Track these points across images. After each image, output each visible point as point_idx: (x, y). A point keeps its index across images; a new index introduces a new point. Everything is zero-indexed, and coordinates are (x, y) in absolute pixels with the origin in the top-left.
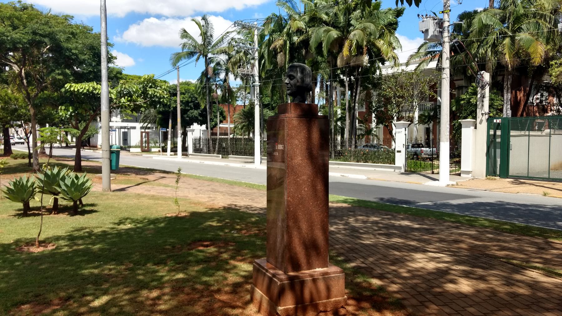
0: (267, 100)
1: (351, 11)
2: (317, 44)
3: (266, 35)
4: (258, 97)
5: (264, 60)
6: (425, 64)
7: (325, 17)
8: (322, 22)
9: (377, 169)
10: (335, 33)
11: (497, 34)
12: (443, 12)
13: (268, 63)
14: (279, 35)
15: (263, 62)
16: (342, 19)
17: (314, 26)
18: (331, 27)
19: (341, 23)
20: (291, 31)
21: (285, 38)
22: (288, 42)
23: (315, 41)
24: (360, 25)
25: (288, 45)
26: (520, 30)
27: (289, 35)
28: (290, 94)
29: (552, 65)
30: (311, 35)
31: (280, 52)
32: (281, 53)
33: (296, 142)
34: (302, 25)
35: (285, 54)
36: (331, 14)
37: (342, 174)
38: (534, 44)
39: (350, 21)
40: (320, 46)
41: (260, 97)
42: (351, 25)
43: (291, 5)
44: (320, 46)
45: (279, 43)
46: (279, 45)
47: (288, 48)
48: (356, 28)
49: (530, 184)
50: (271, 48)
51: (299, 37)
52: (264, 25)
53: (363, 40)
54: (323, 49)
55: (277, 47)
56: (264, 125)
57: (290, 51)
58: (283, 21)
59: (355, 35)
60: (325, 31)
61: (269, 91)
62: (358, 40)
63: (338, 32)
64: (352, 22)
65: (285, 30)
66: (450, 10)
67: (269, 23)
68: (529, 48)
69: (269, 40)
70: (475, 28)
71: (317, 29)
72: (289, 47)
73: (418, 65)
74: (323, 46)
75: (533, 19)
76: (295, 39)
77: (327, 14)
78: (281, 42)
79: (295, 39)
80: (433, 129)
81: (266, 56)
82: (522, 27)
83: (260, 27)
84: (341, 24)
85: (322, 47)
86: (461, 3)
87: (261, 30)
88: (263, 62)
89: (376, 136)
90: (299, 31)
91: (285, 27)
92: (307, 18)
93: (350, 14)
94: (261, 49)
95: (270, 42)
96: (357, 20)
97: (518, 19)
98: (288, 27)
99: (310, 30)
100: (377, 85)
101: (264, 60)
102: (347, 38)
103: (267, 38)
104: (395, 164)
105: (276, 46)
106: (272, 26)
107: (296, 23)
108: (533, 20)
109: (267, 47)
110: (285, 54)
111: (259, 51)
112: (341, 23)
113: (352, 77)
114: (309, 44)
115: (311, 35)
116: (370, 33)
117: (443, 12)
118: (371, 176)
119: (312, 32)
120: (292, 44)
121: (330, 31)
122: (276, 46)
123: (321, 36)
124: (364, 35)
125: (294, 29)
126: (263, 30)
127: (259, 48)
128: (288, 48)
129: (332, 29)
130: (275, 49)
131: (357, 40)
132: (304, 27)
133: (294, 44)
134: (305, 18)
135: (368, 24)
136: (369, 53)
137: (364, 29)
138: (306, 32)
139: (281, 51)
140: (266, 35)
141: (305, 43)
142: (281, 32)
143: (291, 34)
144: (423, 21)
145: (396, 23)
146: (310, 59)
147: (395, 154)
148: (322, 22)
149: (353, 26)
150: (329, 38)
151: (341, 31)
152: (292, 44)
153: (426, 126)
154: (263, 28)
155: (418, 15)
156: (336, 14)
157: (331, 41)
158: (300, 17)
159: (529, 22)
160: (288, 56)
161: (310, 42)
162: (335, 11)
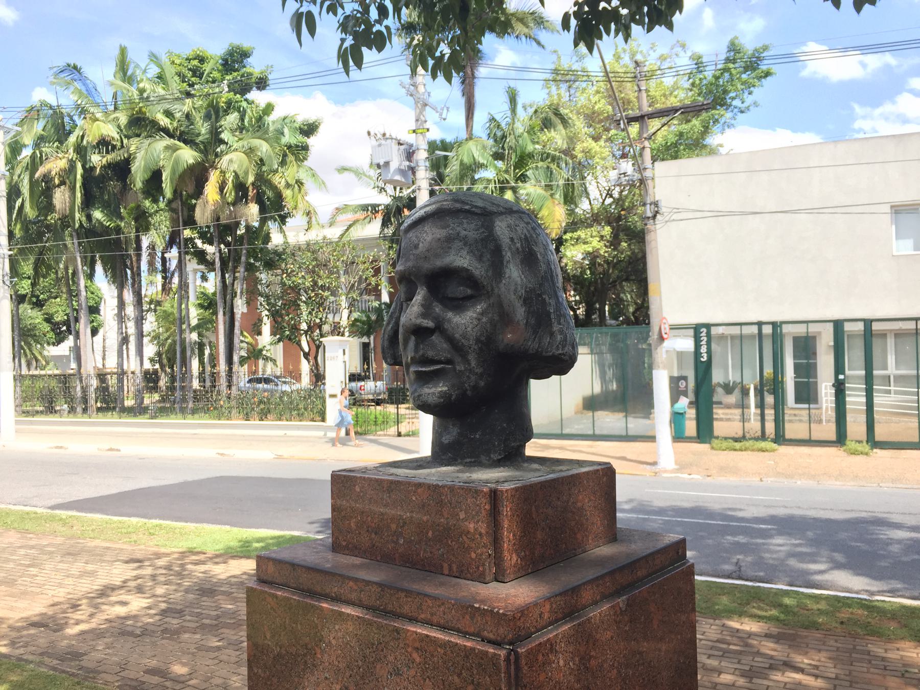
0: (25, 286)
1: (221, 114)
2: (149, 174)
3: (25, 146)
4: (8, 283)
5: (20, 200)
6: (358, 227)
7: (164, 121)
8: (155, 129)
9: (290, 433)
10: (188, 155)
11: (495, 181)
12: (414, 131)
13: (31, 207)
14: (58, 147)
15: (18, 203)
16: (203, 128)
17: (138, 136)
18: (179, 140)
19: (199, 135)
20: (85, 142)
21: (71, 154)
22: (79, 165)
23: (145, 166)
24: (241, 143)
25: (80, 171)
26: (523, 178)
27: (81, 150)
28: (362, 328)
29: (566, 240)
30: (135, 153)
31: (59, 186)
32: (62, 187)
33: (821, 620)
34: (110, 131)
35: (73, 189)
36: (178, 115)
37: (221, 451)
38: (549, 203)
39: (221, 132)
40: (155, 177)
41: (11, 282)
42: (222, 142)
43: (83, 89)
44: (155, 177)
45: (56, 165)
46: (58, 170)
47: (79, 177)
48: (232, 148)
49: (574, 451)
50: (37, 175)
51: (103, 157)
52: (21, 123)
53: (246, 173)
54: (164, 185)
55: (53, 173)
56: (19, 342)
57: (84, 185)
58: (66, 119)
59: (231, 161)
60: (167, 148)
61: (27, 268)
62: (238, 171)
63: (196, 154)
64: (225, 136)
65: (72, 139)
66: (428, 130)
67: (32, 119)
68: (541, 209)
69: (33, 157)
70: (454, 168)
71: (147, 142)
72: (83, 176)
73: (346, 228)
74: (164, 178)
75: (542, 163)
76: (96, 160)
77: (168, 114)
78: (62, 164)
79: (96, 160)
80: (374, 346)
81: (25, 189)
82: (528, 173)
83: (10, 126)
84: (201, 138)
85: (162, 182)
86: (444, 119)
87: (12, 133)
88: (18, 203)
89: (271, 360)
90: (104, 144)
91: (70, 133)
92: (123, 119)
93: (218, 118)
94: (12, 175)
95: (34, 164)
96: (233, 131)
97: (523, 160)
98: (77, 133)
99: (133, 144)
100: (273, 261)
101: (20, 200)
102: (213, 166)
103: (26, 153)
104: (323, 420)
105: (50, 172)
106: (38, 127)
107: (98, 126)
108: (540, 164)
109: (28, 173)
110: (73, 189)
111: (8, 180)
112: (199, 135)
113: (222, 246)
114: (129, 171)
115: (135, 153)
116: (261, 160)
117: (414, 131)
118: (286, 451)
119: (137, 148)
120: (88, 171)
121: (178, 149)
122: (50, 172)
123: (158, 157)
124: (250, 162)
125: (91, 138)
126: (18, 134)
127: (7, 173)
128: (79, 177)
129: (182, 144)
130: (47, 178)
131: (234, 172)
132: (117, 136)
133: (93, 169)
134: (117, 119)
135: (257, 142)
136: (259, 200)
137: (250, 152)
138: (122, 146)
139: (63, 183)
140: (25, 146)
141: (122, 169)
142: (61, 143)
143: (86, 148)
144: (380, 145)
145: (305, 148)
146: (132, 205)
147: (324, 402)
148: (155, 129)
149: (227, 144)
150: (177, 162)
151: (201, 151)
152: (88, 171)
153: (365, 339)
154: (19, 129)
155: (369, 133)
156: (188, 116)
157: (181, 169)
158: (106, 113)
159: (537, 166)
160: (78, 195)
161: (133, 169)
162: (186, 109)
